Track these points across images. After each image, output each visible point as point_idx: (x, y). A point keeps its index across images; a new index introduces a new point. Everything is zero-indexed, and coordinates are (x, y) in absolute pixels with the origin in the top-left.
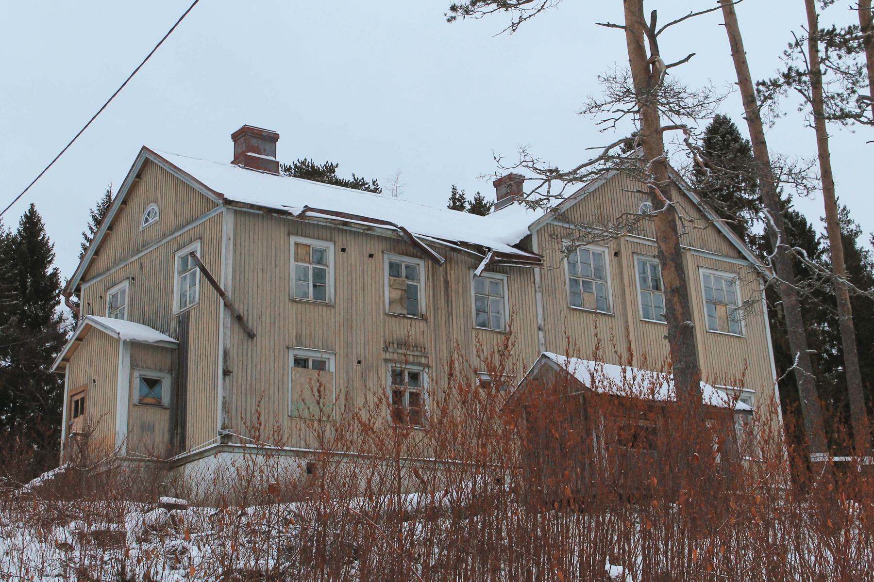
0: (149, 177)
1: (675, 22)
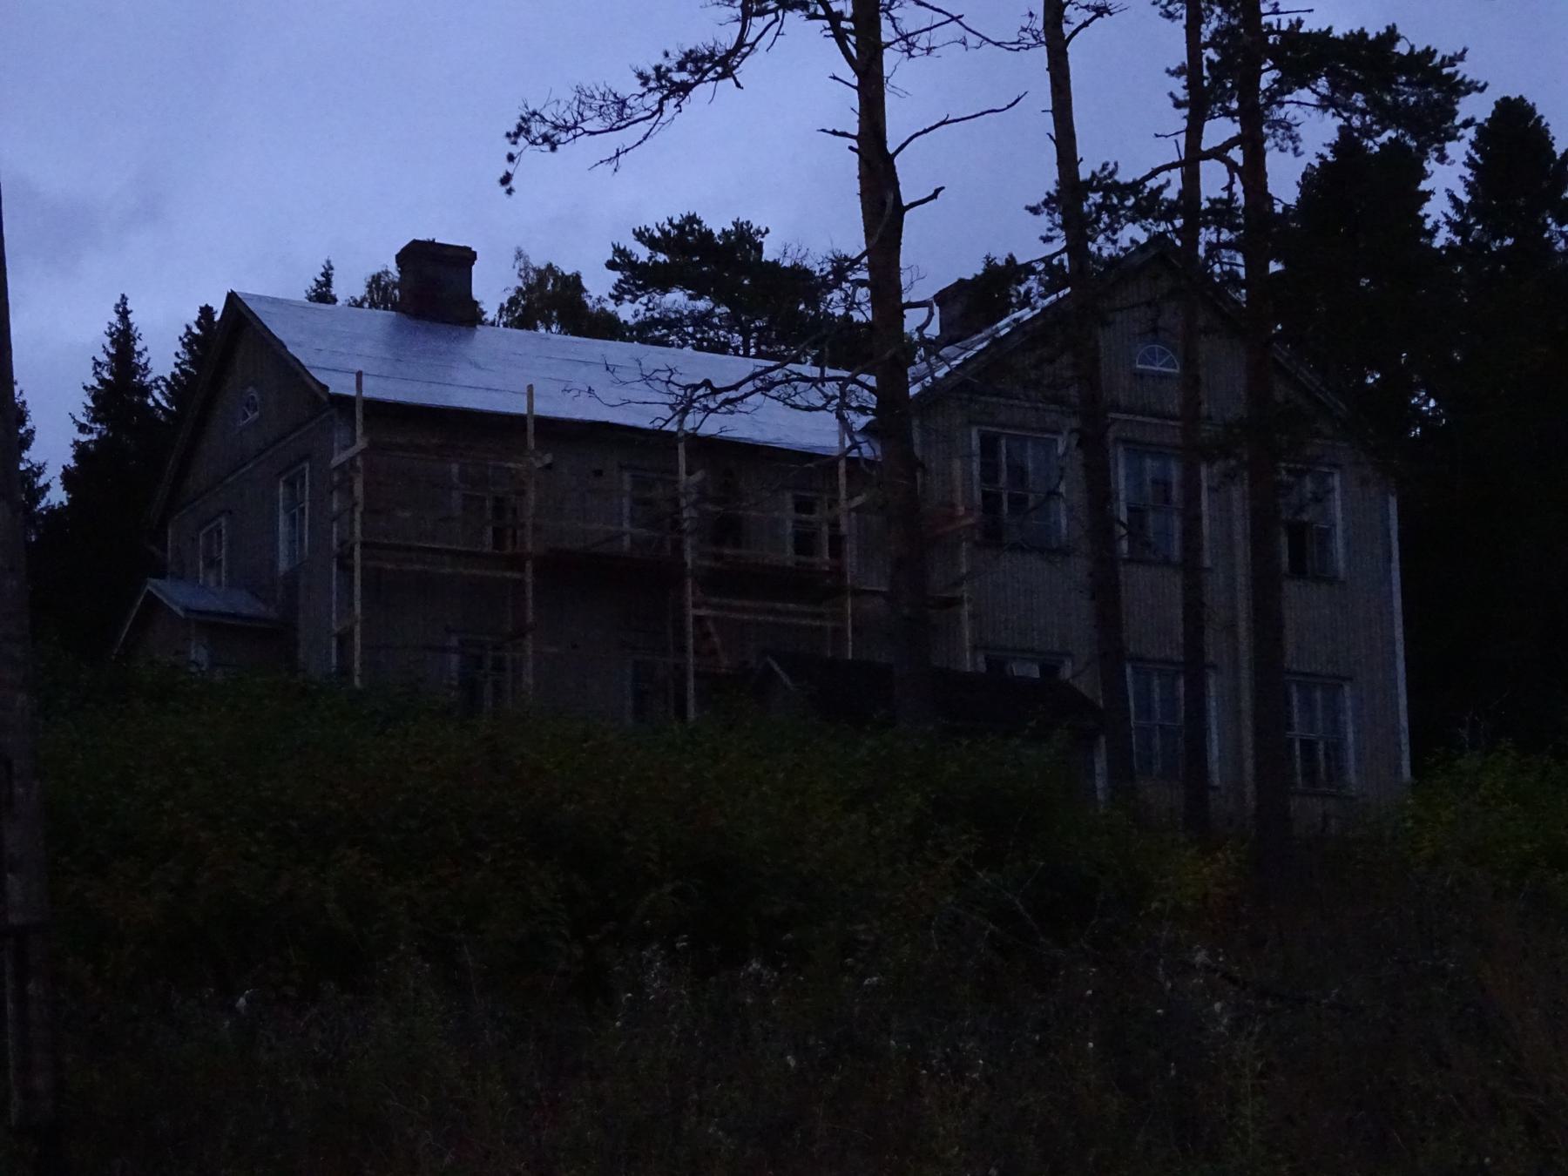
1: (925, 131)
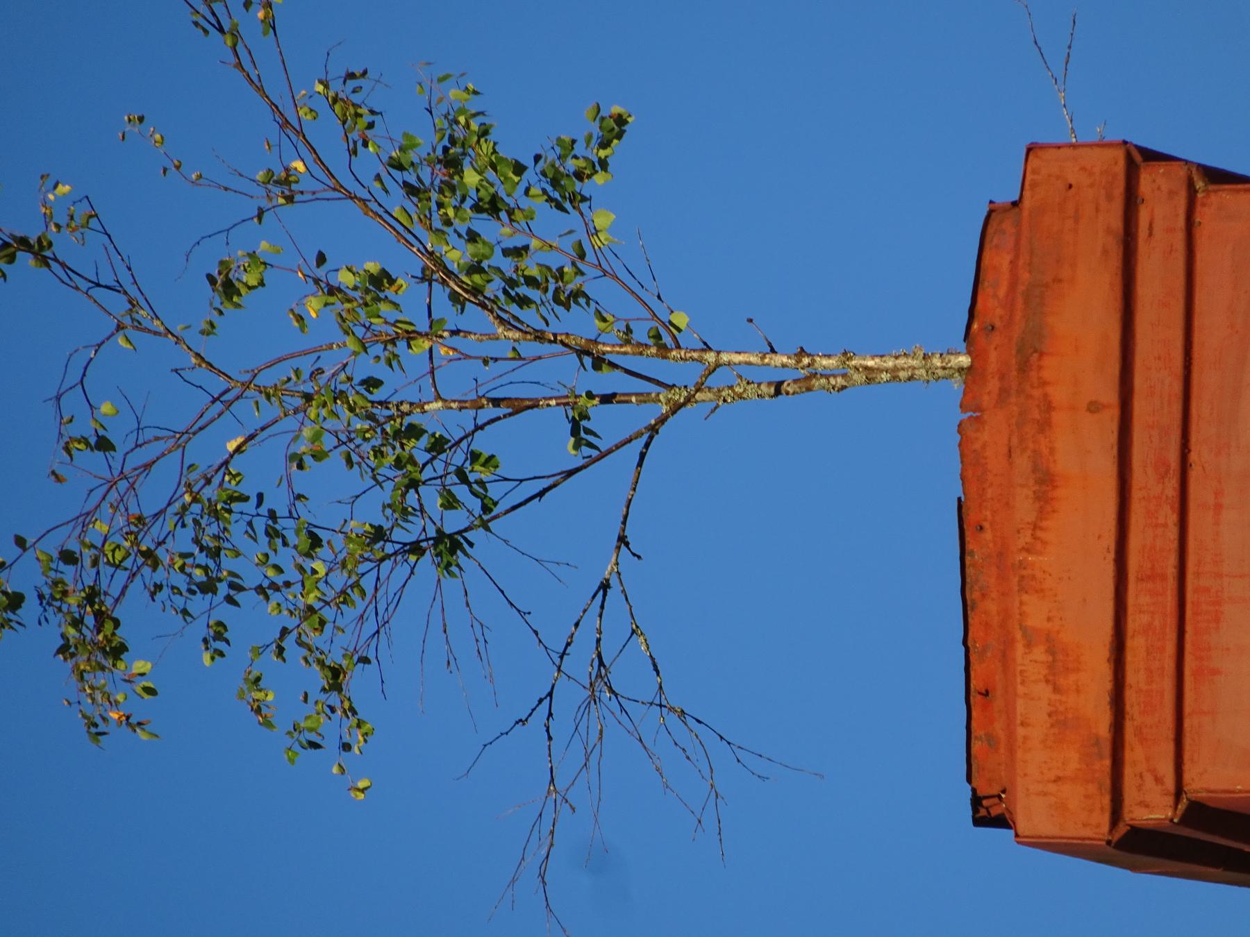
0: (993, 215)
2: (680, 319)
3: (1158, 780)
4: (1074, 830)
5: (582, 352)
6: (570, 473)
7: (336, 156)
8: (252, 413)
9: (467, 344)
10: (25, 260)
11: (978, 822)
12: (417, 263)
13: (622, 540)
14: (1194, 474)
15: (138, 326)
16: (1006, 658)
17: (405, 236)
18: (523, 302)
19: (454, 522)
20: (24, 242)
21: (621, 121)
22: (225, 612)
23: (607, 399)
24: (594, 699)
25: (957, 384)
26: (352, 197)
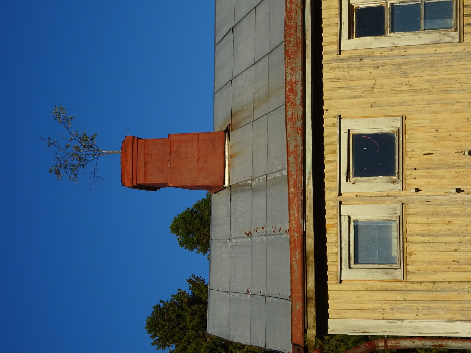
2: (100, 149)
3: (135, 182)
4: (129, 186)
5: (93, 151)
6: (92, 160)
7: (75, 136)
8: (69, 156)
9: (85, 151)
10: (52, 145)
11: (122, 185)
12: (81, 145)
13: (96, 165)
14: (138, 160)
15: (60, 149)
16: (124, 173)
17: (80, 143)
18: (89, 147)
19: (84, 164)
20: (52, 144)
21: (96, 134)
22: (67, 171)
23: (95, 154)
24: (94, 176)
25: (120, 153)
26: (76, 140)
